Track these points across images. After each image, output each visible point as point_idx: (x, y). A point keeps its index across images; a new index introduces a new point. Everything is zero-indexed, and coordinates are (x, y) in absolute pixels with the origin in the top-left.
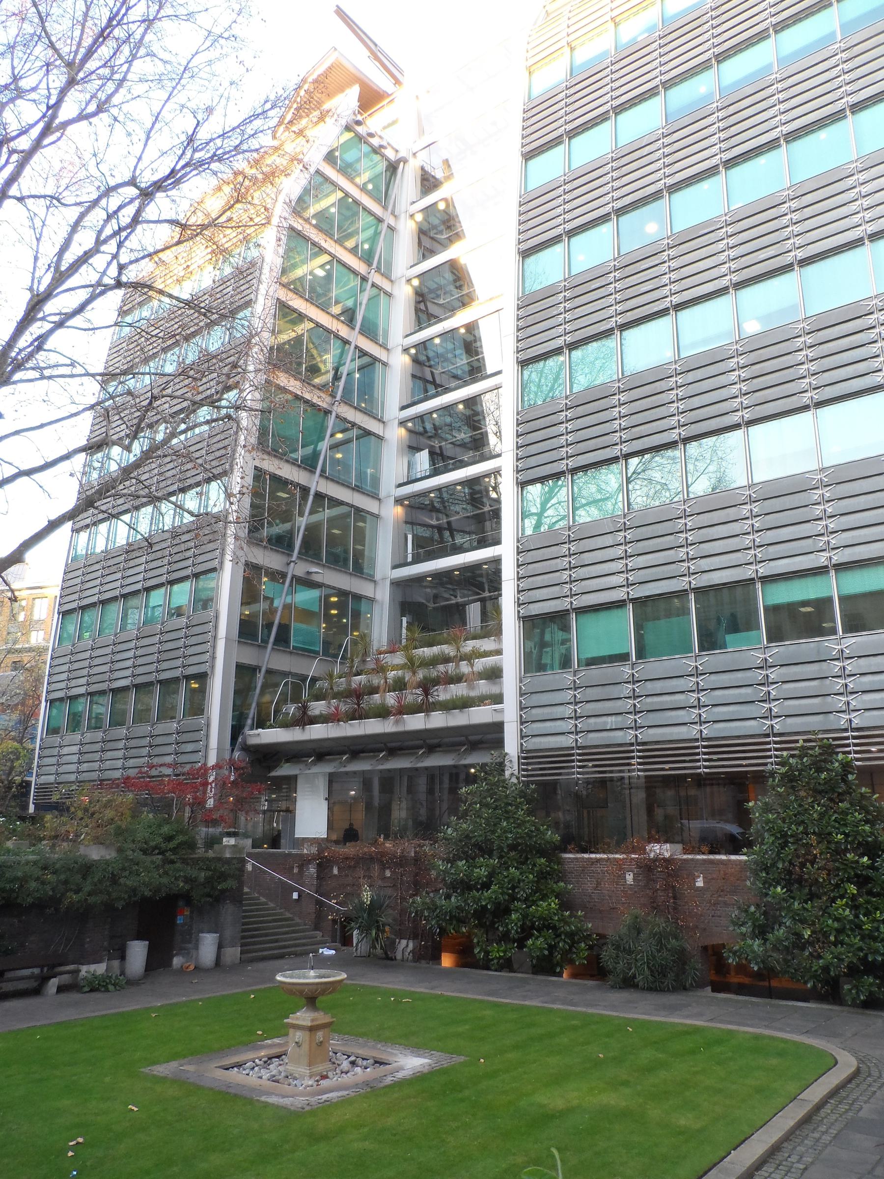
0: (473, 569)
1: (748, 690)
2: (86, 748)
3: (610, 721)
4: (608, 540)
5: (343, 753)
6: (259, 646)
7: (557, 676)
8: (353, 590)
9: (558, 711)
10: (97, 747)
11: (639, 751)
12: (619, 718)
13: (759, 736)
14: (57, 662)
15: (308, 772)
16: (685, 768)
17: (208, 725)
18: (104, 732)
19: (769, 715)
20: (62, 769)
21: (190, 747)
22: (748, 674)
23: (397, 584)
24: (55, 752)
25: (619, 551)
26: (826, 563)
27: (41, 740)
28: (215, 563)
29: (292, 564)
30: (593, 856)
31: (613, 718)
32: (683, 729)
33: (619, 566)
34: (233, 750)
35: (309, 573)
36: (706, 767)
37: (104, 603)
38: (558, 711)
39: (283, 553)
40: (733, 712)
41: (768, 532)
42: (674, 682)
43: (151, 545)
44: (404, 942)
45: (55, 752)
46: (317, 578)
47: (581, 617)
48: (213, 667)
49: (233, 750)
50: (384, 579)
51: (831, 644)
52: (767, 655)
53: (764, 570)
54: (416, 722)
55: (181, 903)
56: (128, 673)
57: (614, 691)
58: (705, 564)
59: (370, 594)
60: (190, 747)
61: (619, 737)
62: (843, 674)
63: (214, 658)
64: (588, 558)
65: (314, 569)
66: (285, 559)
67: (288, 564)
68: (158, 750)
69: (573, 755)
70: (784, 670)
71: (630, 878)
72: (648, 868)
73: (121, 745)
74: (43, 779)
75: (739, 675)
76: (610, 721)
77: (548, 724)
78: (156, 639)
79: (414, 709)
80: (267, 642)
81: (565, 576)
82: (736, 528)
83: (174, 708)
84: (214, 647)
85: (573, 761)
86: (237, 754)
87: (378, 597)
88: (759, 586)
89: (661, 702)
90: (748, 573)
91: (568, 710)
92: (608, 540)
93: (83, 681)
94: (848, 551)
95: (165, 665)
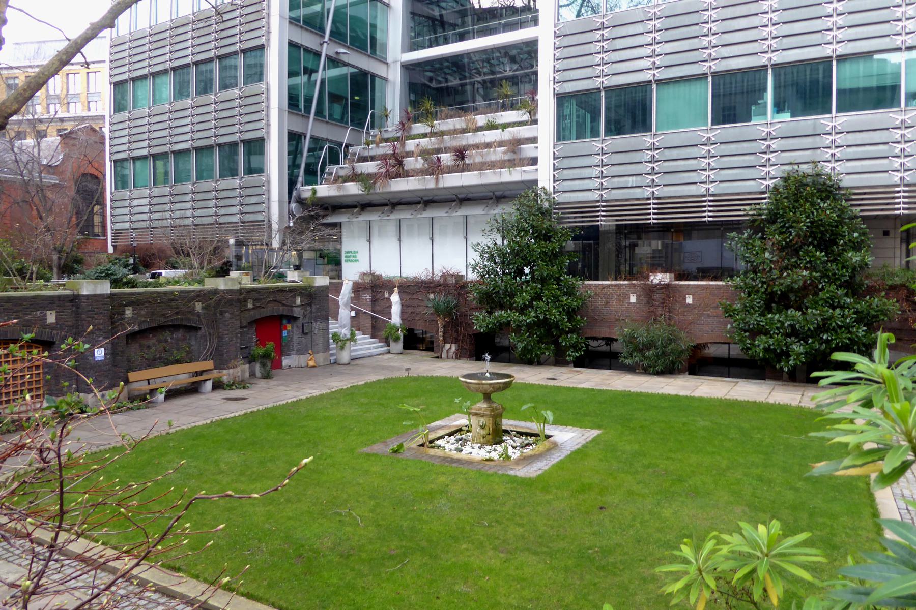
0: (505, 51)
1: (752, 157)
2: (155, 201)
3: (631, 181)
4: (639, 28)
5: (355, 207)
6: (303, 116)
7: (586, 144)
8: (371, 70)
9: (586, 173)
10: (167, 199)
11: (603, 206)
12: (639, 178)
13: (755, 193)
14: (115, 127)
15: (419, 216)
16: (626, 220)
17: (269, 182)
18: (171, 187)
19: (653, 184)
20: (134, 218)
21: (254, 200)
22: (753, 144)
23: (408, 68)
24: (127, 203)
25: (648, 38)
26: (831, 54)
27: (111, 193)
28: (263, 40)
29: (325, 45)
30: (600, 282)
31: (634, 178)
32: (693, 187)
33: (647, 51)
34: (289, 202)
35: (337, 53)
36: (654, 219)
37: (155, 75)
38: (586, 173)
39: (316, 34)
40: (737, 174)
41: (785, 26)
42: (689, 150)
43: (218, 13)
44: (448, 346)
45: (127, 203)
46: (344, 58)
47: (661, 87)
48: (268, 133)
49: (289, 202)
50: (395, 62)
51: (825, 121)
52: (655, 141)
53: (842, 49)
54: (452, 180)
55: (284, 322)
56: (125, 147)
57: (636, 157)
58: (726, 52)
59: (384, 75)
60: (254, 200)
61: (638, 193)
62: (834, 145)
63: (268, 125)
64: (620, 44)
65: (342, 50)
66: (318, 40)
67: (322, 44)
68: (223, 203)
69: (598, 207)
70: (784, 142)
71: (633, 299)
72: (650, 291)
73: (189, 197)
74: (118, 226)
75: (745, 145)
76: (631, 181)
77: (577, 182)
78: (145, 121)
79: (502, 164)
80: (309, 113)
81: (597, 59)
82: (755, 21)
83: (211, 170)
84: (268, 116)
85: (598, 211)
86: (293, 205)
87: (390, 77)
88: (654, 87)
89: (677, 166)
90: (828, 51)
91: (596, 172)
92: (639, 28)
93: (145, 144)
94: (851, 44)
95: (135, 146)
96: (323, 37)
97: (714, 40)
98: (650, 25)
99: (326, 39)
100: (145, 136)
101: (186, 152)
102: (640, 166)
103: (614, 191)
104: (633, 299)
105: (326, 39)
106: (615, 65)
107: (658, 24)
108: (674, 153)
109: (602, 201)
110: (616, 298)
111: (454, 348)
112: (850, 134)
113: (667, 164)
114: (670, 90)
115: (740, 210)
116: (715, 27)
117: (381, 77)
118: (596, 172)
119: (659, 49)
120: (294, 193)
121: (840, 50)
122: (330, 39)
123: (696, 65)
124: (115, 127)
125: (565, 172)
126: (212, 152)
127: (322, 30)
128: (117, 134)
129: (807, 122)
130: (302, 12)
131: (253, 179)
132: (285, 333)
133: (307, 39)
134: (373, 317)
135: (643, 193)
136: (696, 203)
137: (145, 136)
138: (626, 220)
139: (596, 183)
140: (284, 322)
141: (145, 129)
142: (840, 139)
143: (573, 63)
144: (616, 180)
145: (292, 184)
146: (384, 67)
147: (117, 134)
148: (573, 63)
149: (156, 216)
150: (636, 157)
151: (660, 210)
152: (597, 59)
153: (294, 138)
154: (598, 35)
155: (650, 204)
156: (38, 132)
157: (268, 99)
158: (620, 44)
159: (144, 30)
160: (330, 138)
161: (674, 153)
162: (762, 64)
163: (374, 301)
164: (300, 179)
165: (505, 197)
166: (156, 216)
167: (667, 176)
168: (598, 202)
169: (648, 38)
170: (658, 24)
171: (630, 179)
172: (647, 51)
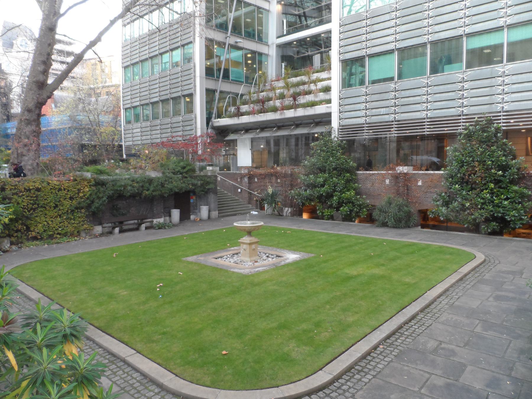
1: (453, 94)
2: (144, 130)
3: (383, 111)
4: (387, 17)
5: (257, 129)
10: (148, 129)
12: (387, 109)
14: (125, 91)
16: (417, 132)
17: (196, 118)
22: (454, 85)
23: (280, 46)
25: (392, 23)
27: (124, 126)
28: (191, 39)
29: (228, 38)
31: (384, 109)
32: (418, 113)
35: (236, 42)
37: (142, 61)
40: (521, 96)
42: (416, 91)
43: (160, 31)
44: (287, 209)
45: (130, 132)
46: (240, 45)
48: (195, 90)
50: (273, 44)
51: (499, 69)
52: (464, 76)
54: (290, 114)
55: (192, 194)
57: (386, 96)
61: (386, 118)
62: (503, 84)
63: (195, 86)
64: (376, 27)
67: (226, 38)
69: (364, 127)
71: (387, 181)
72: (396, 177)
73: (158, 127)
74: (127, 144)
75: (449, 86)
76: (383, 111)
77: (353, 113)
80: (219, 78)
83: (180, 111)
84: (195, 81)
86: (209, 130)
87: (270, 53)
88: (367, 59)
89: (409, 101)
90: (460, 32)
91: (363, 106)
96: (227, 33)
97: (431, 21)
98: (393, 15)
99: (229, 35)
100: (138, 95)
101: (157, 102)
102: (388, 101)
103: (373, 118)
104: (387, 181)
105: (229, 35)
106: (373, 41)
107: (398, 14)
108: (408, 93)
109: (367, 124)
110: (377, 182)
111: (290, 210)
112: (514, 76)
113: (403, 100)
114: (376, 60)
115: (417, 129)
116: (431, 13)
117: (265, 54)
118: (363, 106)
119: (398, 29)
120: (210, 124)
121: (509, 21)
122: (231, 35)
123: (420, 38)
124: (125, 91)
125: (346, 107)
126: (169, 104)
127: (226, 29)
128: (126, 94)
129: (486, 70)
130: (214, 22)
131: (188, 116)
132: (192, 201)
133: (218, 36)
134: (249, 192)
135: (390, 117)
136: (420, 123)
137: (138, 95)
138: (417, 132)
139: (363, 113)
140: (192, 194)
141: (138, 91)
142: (507, 80)
143: (350, 41)
144: (374, 110)
145: (209, 120)
146: (267, 47)
147: (126, 94)
148: (350, 41)
149: (144, 138)
150: (386, 96)
151: (399, 129)
152: (364, 38)
153: (210, 93)
154: (364, 23)
155: (393, 125)
156: (97, 94)
157: (195, 71)
158: (376, 27)
159: (146, 33)
160: (232, 91)
161: (408, 93)
162: (459, 34)
163: (250, 183)
164: (214, 115)
165: (283, 126)
166: (144, 138)
167: (403, 107)
168: (364, 124)
169: (392, 23)
170: (398, 14)
171: (382, 110)
172: (392, 31)
